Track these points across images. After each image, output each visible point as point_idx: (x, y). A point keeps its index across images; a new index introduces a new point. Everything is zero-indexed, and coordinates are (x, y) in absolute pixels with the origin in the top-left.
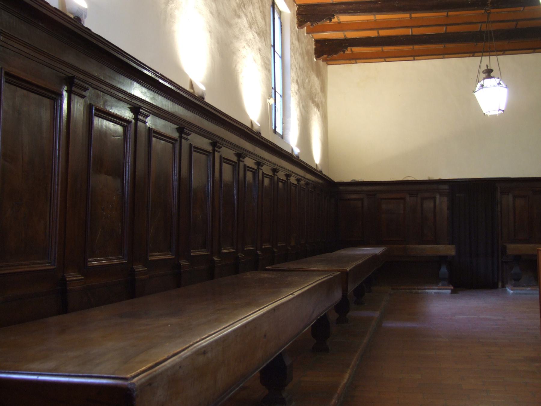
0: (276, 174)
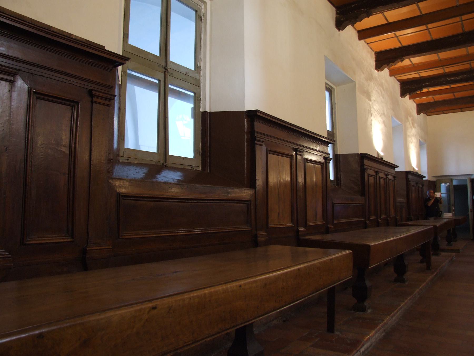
0: (377, 174)
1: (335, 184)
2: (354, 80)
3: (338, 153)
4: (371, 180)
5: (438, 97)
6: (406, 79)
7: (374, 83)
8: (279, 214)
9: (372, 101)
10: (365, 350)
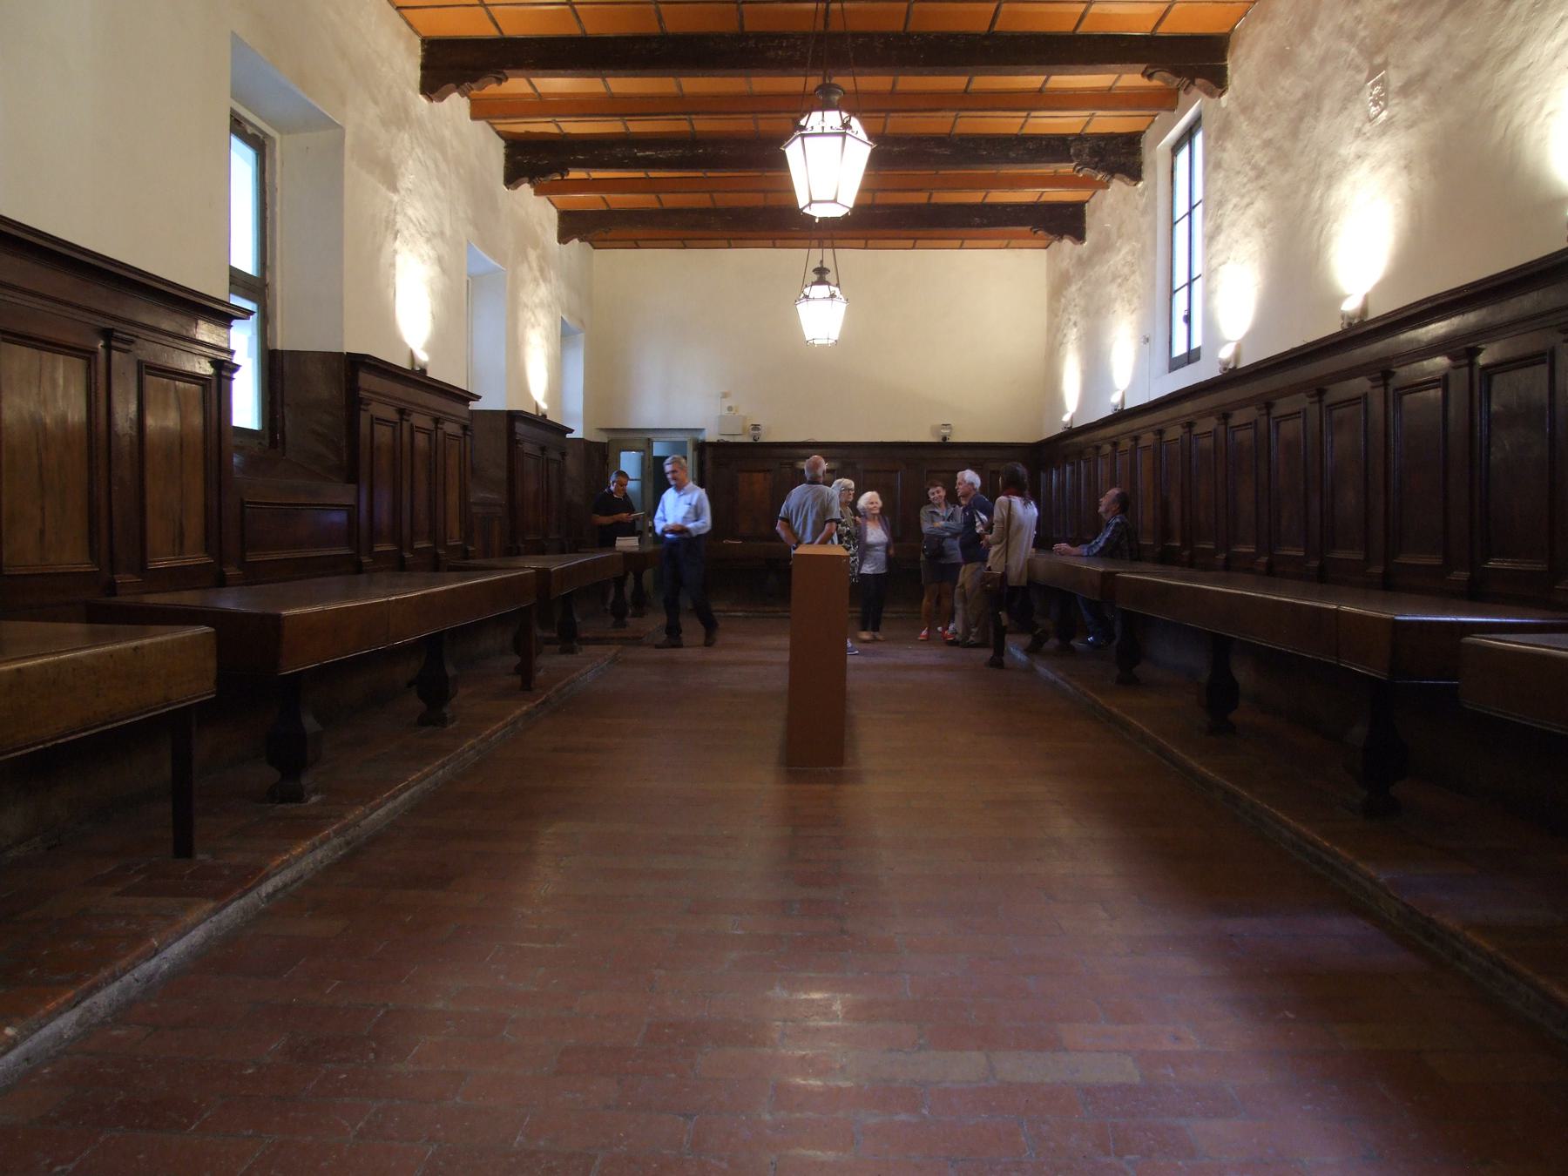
1: (266, 442)
2: (337, 122)
3: (279, 348)
4: (383, 434)
5: (619, 200)
6: (522, 134)
7: (411, 138)
8: (42, 532)
9: (403, 192)
10: (276, 892)
